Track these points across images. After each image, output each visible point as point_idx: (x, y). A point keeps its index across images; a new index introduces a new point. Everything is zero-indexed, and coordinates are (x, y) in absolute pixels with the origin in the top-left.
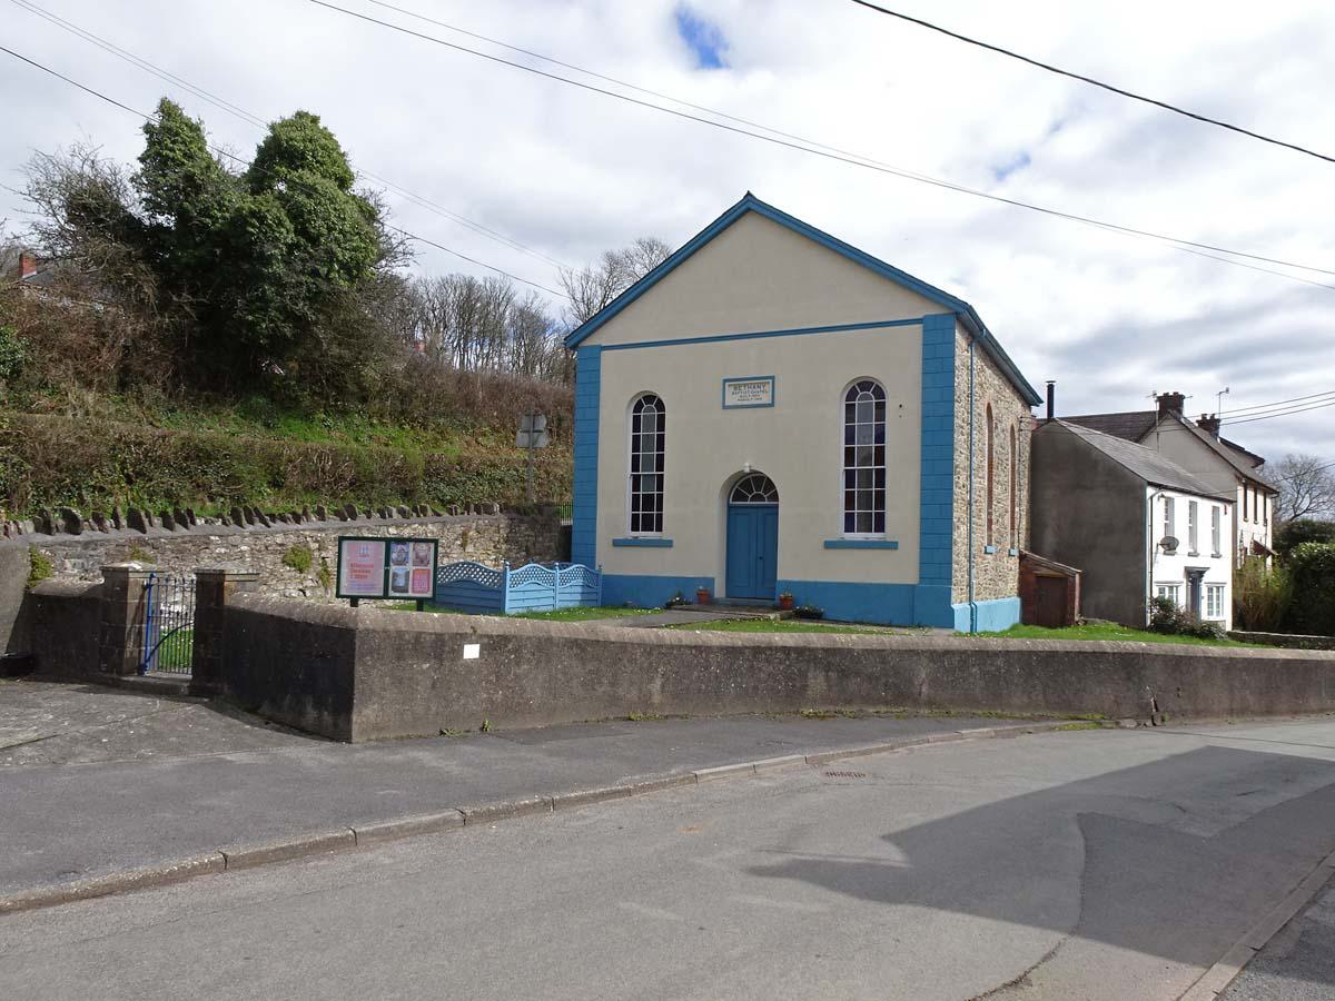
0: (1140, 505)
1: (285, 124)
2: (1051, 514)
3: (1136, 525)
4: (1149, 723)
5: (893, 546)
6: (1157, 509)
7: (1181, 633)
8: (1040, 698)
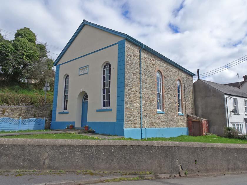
0: (223, 100)
1: (22, 29)
2: (200, 104)
3: (223, 106)
4: (177, 175)
5: (111, 110)
6: (230, 104)
7: (236, 138)
8: (116, 164)
